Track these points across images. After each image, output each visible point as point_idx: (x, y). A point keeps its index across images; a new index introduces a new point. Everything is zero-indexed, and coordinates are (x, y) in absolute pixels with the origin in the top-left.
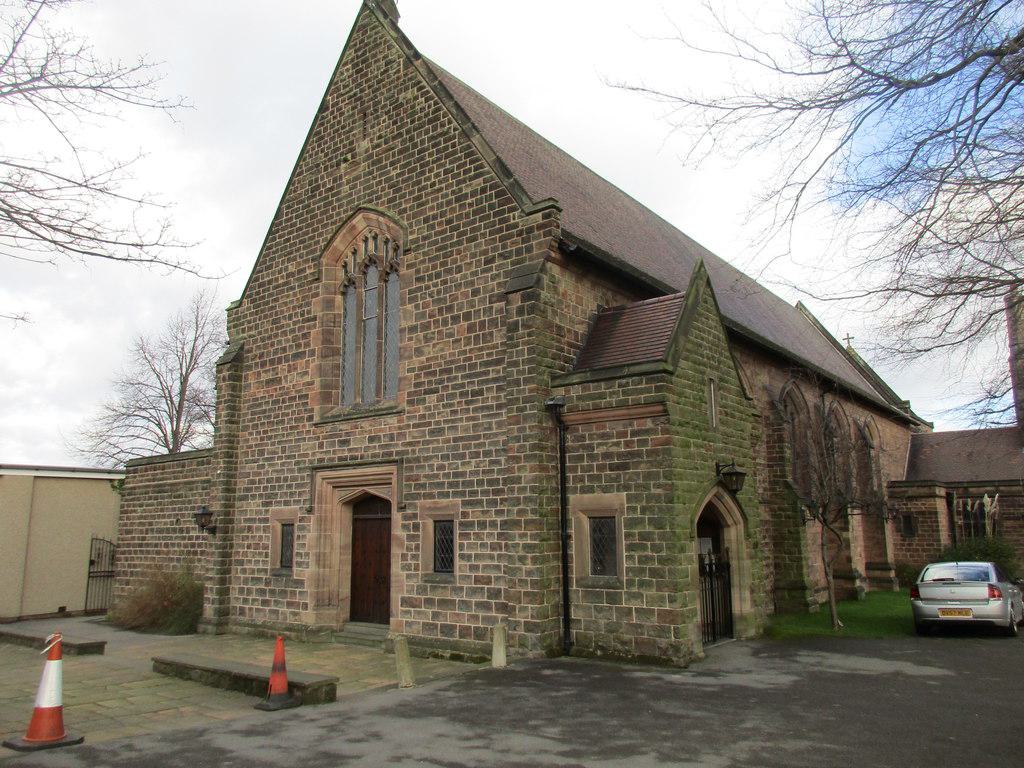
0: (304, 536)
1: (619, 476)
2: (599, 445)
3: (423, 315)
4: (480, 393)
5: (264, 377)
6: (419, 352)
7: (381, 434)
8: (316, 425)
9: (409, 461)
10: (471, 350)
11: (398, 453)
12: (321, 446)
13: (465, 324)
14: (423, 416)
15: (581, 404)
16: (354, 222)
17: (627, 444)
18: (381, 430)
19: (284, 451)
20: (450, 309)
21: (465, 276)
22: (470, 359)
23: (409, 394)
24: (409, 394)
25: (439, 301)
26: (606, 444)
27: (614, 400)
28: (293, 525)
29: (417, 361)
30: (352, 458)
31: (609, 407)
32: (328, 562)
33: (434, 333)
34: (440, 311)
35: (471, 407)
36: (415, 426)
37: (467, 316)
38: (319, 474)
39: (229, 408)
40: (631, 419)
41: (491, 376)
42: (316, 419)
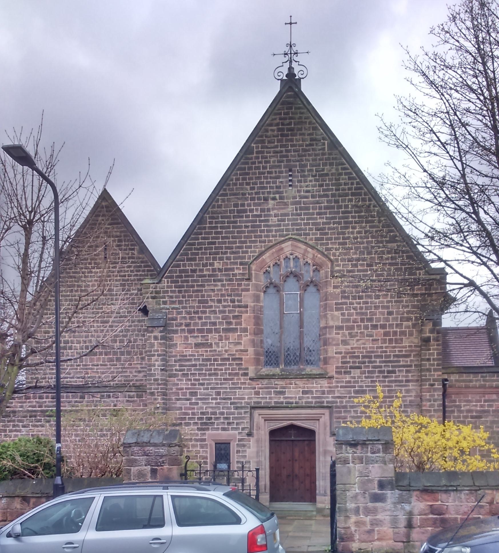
0: (246, 451)
1: (476, 422)
2: (464, 406)
3: (348, 320)
4: (394, 372)
5: (191, 341)
6: (345, 342)
7: (314, 390)
8: (251, 379)
9: (337, 407)
10: (386, 347)
11: (327, 402)
12: (257, 393)
13: (382, 331)
14: (350, 382)
15: (458, 384)
16: (283, 245)
17: (482, 406)
18: (313, 387)
19: (218, 394)
20: (370, 320)
21: (382, 302)
22: (386, 352)
23: (337, 368)
24: (337, 368)
25: (362, 314)
26: (469, 405)
27: (478, 384)
28: (230, 443)
29: (342, 348)
30: (287, 403)
31: (475, 387)
32: (14, 477)
33: (357, 333)
34: (362, 320)
35: (387, 379)
36: (341, 387)
37: (383, 327)
38: (257, 411)
39: (162, 360)
40: (484, 394)
41: (401, 363)
42: (251, 374)
